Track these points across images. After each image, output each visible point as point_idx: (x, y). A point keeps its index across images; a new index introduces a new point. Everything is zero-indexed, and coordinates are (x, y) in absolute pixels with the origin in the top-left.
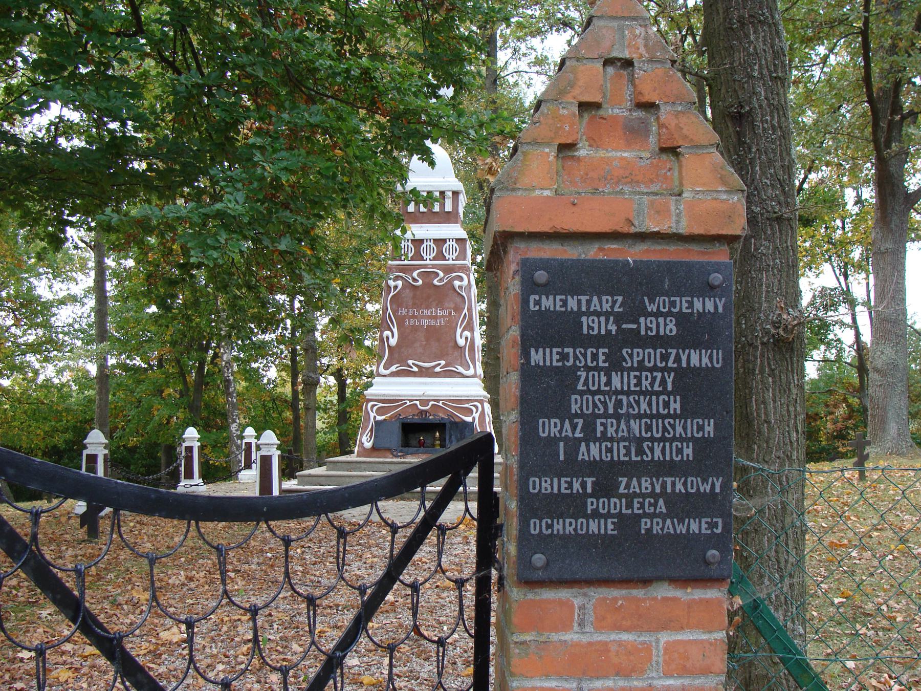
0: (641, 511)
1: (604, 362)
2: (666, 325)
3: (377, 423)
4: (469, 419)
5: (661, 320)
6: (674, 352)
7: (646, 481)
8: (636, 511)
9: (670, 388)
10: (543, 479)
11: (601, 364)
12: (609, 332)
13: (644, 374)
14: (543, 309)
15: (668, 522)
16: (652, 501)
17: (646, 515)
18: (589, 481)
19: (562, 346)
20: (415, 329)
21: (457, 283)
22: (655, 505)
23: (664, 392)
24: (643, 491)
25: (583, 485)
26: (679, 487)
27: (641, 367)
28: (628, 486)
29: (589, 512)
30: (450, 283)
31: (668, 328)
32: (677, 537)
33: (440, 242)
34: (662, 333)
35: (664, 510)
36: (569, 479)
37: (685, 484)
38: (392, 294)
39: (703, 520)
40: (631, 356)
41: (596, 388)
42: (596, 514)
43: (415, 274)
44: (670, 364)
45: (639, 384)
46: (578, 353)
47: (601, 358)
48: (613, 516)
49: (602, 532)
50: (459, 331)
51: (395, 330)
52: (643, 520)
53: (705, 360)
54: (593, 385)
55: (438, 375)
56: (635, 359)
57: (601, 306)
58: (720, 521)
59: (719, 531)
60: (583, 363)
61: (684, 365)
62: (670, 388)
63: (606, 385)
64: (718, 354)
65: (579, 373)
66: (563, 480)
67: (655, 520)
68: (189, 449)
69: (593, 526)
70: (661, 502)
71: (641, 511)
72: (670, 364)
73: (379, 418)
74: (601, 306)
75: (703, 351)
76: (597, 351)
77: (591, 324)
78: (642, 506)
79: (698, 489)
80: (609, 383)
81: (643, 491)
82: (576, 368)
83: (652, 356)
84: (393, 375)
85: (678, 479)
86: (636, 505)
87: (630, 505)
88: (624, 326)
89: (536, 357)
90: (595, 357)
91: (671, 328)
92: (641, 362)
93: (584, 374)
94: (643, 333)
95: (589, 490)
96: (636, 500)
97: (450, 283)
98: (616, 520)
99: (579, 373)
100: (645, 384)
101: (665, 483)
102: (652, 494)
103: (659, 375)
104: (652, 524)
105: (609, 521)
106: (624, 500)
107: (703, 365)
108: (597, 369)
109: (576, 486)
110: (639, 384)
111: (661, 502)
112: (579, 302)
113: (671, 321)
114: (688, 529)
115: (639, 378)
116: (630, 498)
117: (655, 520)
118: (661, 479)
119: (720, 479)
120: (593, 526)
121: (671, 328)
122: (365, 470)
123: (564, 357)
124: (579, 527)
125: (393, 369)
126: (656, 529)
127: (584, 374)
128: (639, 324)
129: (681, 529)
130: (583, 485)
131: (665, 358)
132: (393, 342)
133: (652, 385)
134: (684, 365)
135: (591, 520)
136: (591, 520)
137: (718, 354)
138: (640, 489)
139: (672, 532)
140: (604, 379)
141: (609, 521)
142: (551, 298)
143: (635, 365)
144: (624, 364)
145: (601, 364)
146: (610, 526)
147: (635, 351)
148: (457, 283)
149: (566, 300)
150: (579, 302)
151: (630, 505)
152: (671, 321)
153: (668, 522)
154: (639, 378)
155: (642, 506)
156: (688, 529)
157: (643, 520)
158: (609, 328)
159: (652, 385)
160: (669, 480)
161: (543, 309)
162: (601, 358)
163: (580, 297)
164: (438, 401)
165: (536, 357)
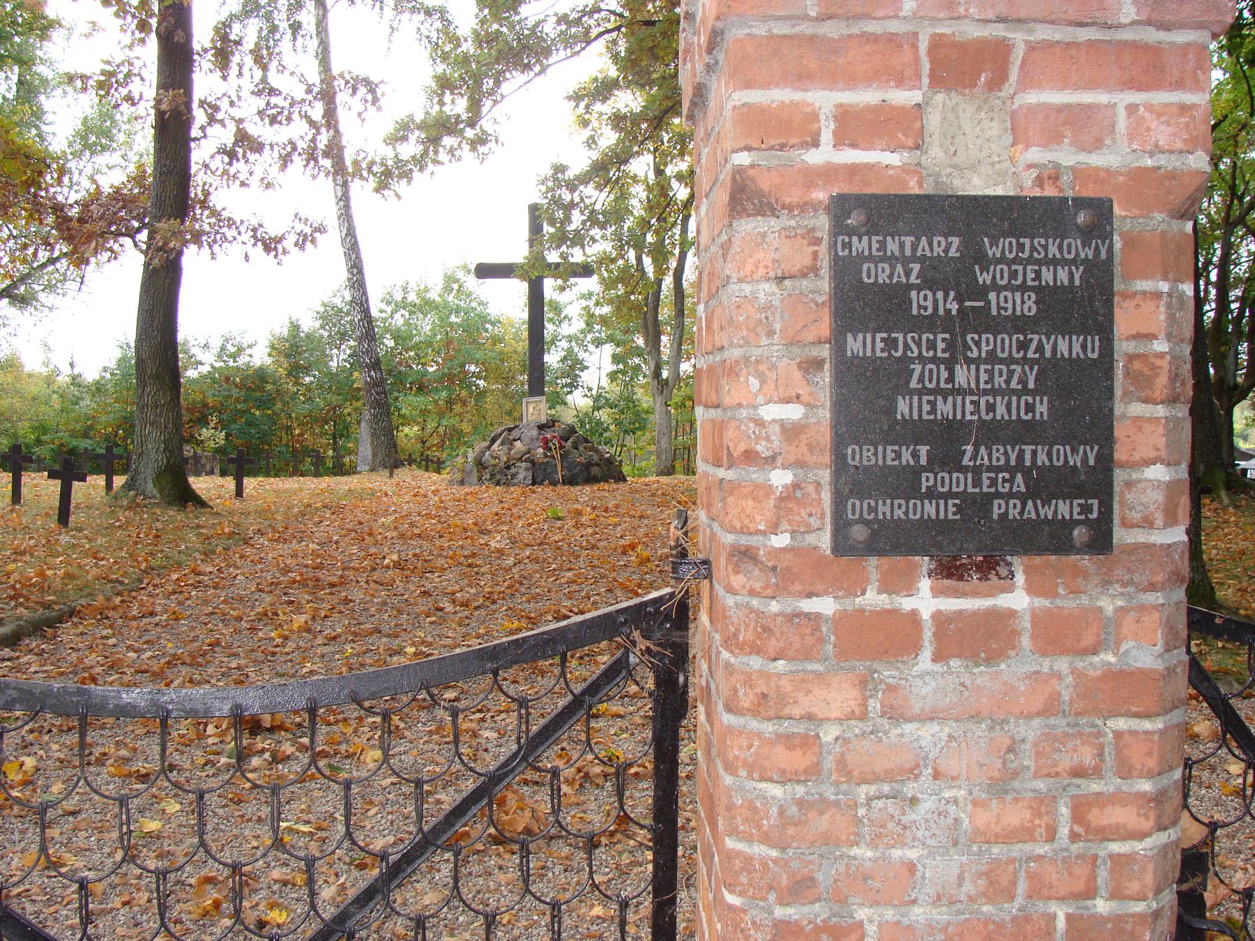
0: (992, 490)
1: (944, 351)
2: (1023, 302)
5: (1018, 295)
6: (1036, 337)
7: (998, 450)
8: (985, 490)
9: (1031, 386)
10: (865, 447)
11: (939, 354)
12: (948, 311)
13: (997, 367)
14: (854, 254)
15: (1030, 503)
16: (1007, 476)
17: (998, 495)
18: (923, 450)
19: (889, 331)
22: (1011, 481)
23: (1025, 391)
24: (994, 462)
25: (915, 455)
26: (1042, 459)
27: (992, 358)
28: (974, 457)
29: (923, 490)
31: (1026, 307)
32: (1041, 522)
34: (1019, 313)
35: (1023, 489)
36: (897, 448)
37: (1049, 455)
39: (1076, 502)
40: (978, 344)
41: (946, 489)
42: (931, 494)
44: (1030, 355)
45: (990, 380)
46: (909, 340)
47: (941, 346)
48: (956, 495)
49: (942, 516)
52: (996, 502)
53: (1077, 348)
54: (930, 381)
56: (984, 348)
57: (932, 250)
58: (1095, 502)
59: (1094, 515)
60: (916, 354)
61: (1048, 354)
62: (1031, 386)
63: (947, 382)
64: (1093, 341)
65: (912, 366)
66: (889, 448)
67: (1011, 502)
69: (930, 509)
70: (1019, 478)
71: (992, 490)
72: (1030, 355)
74: (932, 250)
75: (1074, 337)
76: (935, 337)
77: (922, 303)
78: (993, 482)
79: (1066, 461)
80: (951, 379)
81: (994, 462)
82: (905, 360)
83: (1008, 343)
85: (1039, 447)
86: (986, 482)
87: (977, 483)
88: (967, 304)
89: (854, 345)
90: (932, 345)
91: (1029, 306)
92: (992, 353)
93: (918, 368)
94: (994, 312)
95: (923, 461)
96: (985, 475)
98: (957, 501)
99: (912, 366)
100: (999, 381)
101: (1022, 452)
102: (1006, 467)
103: (1018, 369)
104: (1007, 507)
105: (950, 502)
106: (970, 475)
107: (1074, 355)
108: (935, 360)
109: (906, 456)
110: (990, 380)
111: (1019, 478)
112: (902, 245)
113: (1029, 297)
114: (1055, 512)
115: (990, 373)
116: (977, 471)
117: (1011, 502)
118: (1017, 448)
119: (1096, 448)
120: (930, 509)
121: (1029, 306)
123: (891, 344)
124: (911, 510)
126: (1013, 513)
127: (918, 368)
128: (989, 302)
129: (1047, 512)
130: (915, 455)
131: (1023, 346)
133: (1008, 382)
134: (1048, 354)
135: (926, 501)
136: (926, 501)
137: (1093, 341)
138: (990, 459)
139: (1033, 516)
140: (944, 375)
141: (950, 502)
142: (865, 239)
143: (983, 355)
144: (969, 353)
145: (939, 354)
146: (951, 509)
147: (984, 337)
149: (885, 241)
150: (902, 245)
151: (977, 483)
152: (1029, 297)
153: (1030, 503)
154: (990, 373)
155: (993, 482)
156: (1055, 512)
157: (996, 502)
158: (948, 306)
159: (1008, 382)
160: (1028, 449)
161: (854, 254)
162: (941, 346)
163: (903, 238)
165: (854, 345)
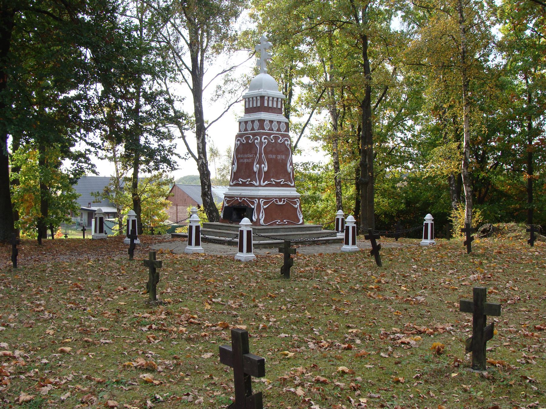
3: (264, 209)
4: (253, 207)
20: (242, 163)
21: (286, 142)
30: (284, 142)
33: (271, 122)
38: (264, 146)
43: (272, 136)
50: (255, 164)
51: (266, 164)
55: (247, 185)
68: (427, 225)
73: (265, 207)
84: (266, 186)
97: (284, 142)
122: (267, 233)
125: (266, 182)
132: (266, 169)
148: (286, 142)
164: (245, 198)
